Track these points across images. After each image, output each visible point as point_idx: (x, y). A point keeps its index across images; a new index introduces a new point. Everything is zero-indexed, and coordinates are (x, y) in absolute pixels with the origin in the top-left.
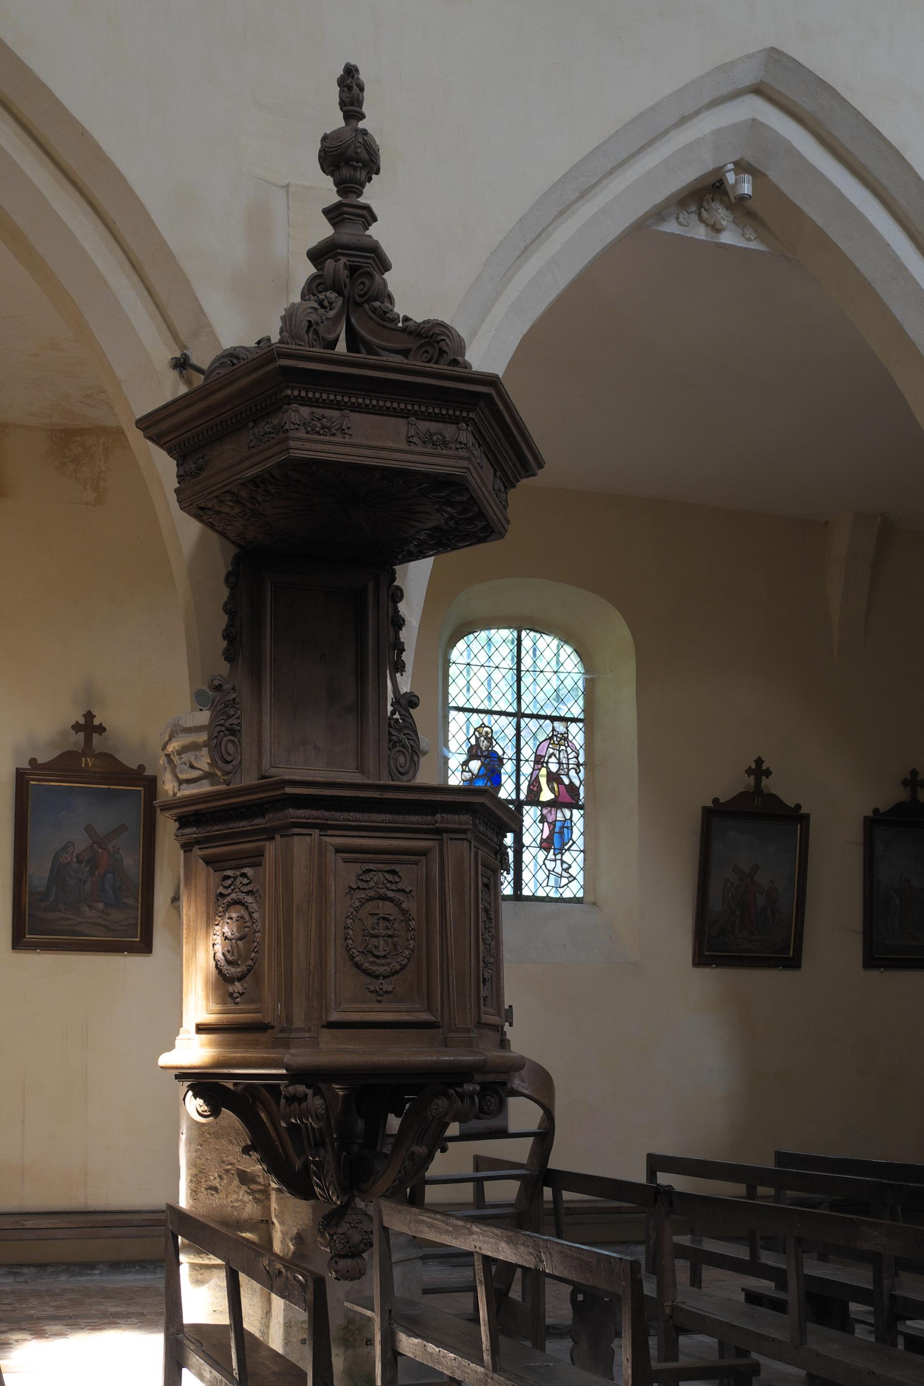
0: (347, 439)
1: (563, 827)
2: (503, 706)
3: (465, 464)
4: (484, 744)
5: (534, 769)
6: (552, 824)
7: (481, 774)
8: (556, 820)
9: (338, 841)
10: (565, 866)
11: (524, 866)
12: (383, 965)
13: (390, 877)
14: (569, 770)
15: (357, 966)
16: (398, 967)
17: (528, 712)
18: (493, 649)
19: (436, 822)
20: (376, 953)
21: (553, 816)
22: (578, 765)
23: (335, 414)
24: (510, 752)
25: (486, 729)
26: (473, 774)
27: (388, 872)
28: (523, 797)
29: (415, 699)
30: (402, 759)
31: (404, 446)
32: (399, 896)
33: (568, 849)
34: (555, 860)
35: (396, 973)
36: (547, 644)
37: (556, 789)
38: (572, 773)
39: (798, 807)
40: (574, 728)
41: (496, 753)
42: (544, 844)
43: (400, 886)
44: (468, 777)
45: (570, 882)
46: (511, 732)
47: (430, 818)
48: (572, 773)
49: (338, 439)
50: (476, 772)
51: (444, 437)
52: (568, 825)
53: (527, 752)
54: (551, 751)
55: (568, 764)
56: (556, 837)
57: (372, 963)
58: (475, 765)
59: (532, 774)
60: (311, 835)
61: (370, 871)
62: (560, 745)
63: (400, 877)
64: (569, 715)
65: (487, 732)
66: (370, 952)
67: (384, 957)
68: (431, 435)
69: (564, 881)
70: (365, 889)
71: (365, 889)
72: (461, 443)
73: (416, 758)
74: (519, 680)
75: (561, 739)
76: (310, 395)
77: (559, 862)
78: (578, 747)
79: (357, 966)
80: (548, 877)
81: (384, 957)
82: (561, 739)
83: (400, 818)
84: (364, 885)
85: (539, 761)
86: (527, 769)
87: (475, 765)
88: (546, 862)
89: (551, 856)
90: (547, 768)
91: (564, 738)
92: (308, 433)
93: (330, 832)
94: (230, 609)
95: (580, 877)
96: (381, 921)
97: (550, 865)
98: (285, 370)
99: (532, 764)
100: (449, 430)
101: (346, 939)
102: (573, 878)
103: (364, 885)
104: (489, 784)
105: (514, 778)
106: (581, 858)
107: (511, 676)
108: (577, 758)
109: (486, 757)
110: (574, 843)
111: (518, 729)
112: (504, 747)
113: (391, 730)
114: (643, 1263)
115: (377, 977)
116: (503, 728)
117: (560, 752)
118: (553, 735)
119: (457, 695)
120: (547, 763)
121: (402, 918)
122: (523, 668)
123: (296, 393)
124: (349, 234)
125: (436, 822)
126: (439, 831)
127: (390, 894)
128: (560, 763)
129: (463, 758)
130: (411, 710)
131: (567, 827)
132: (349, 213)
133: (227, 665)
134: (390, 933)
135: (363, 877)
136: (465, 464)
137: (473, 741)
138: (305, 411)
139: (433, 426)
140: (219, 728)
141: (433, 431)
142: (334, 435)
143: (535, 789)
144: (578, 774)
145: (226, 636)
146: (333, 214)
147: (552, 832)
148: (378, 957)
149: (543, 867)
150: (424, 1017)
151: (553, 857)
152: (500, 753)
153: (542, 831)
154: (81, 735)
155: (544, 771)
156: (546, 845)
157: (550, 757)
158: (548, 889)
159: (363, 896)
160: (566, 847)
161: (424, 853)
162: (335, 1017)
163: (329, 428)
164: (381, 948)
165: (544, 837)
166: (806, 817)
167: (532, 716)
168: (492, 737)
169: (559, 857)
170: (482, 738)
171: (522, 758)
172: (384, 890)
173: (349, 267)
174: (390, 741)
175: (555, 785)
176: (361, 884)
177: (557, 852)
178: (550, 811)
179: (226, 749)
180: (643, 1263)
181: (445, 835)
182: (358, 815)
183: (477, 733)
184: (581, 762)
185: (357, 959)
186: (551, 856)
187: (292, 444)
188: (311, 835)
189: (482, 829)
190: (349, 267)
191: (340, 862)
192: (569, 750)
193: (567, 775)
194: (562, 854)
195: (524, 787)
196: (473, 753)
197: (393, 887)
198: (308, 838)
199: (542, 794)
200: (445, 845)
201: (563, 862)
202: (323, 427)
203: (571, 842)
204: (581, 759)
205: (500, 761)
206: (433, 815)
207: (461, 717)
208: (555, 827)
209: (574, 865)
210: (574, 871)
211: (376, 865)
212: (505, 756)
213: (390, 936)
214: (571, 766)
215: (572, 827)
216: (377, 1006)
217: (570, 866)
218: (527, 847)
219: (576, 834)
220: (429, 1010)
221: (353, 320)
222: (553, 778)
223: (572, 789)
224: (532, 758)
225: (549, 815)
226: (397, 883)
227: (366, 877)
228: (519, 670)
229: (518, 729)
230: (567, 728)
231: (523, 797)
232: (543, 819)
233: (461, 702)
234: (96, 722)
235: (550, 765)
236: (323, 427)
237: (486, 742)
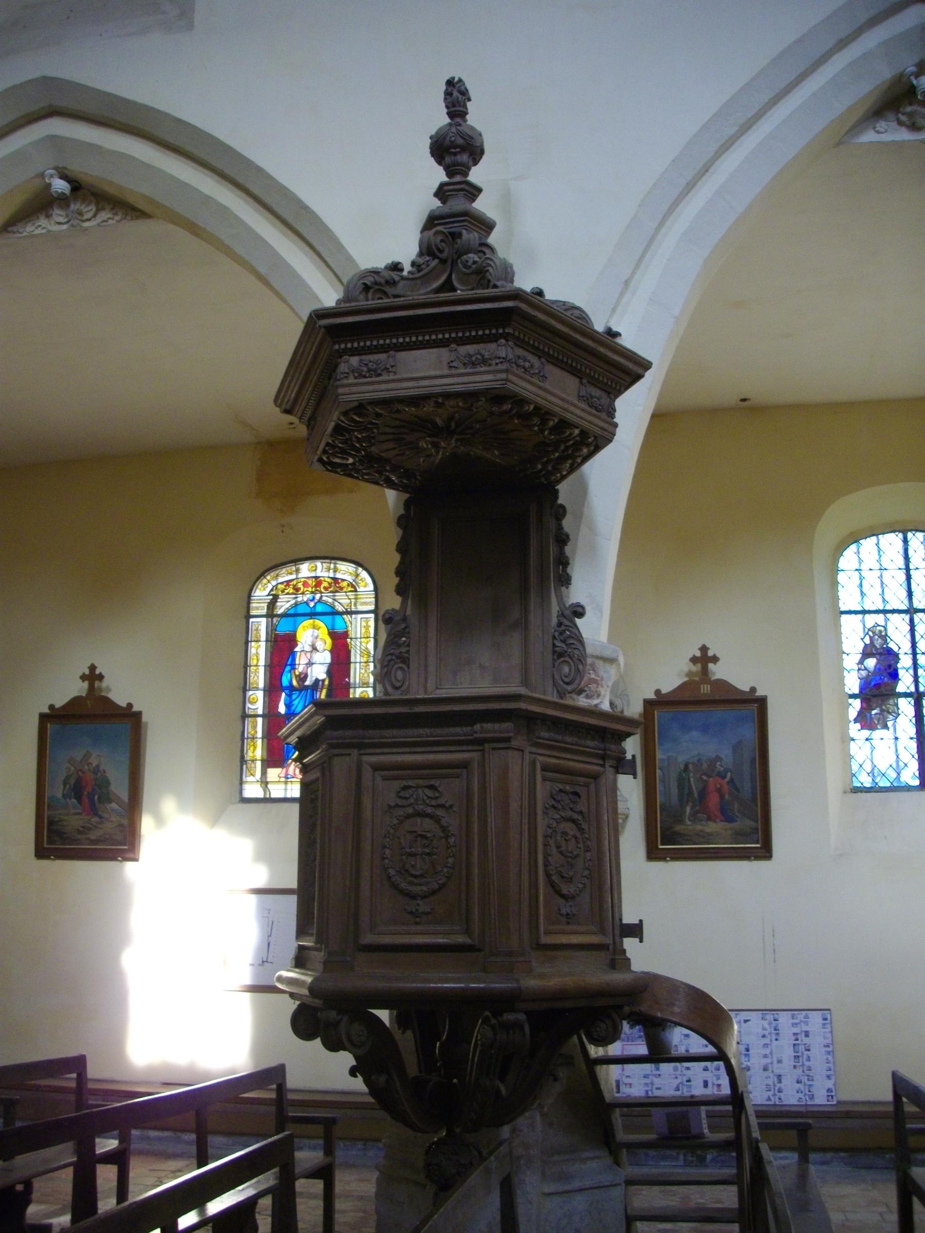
0: (392, 377)
3: (504, 376)
4: (878, 643)
9: (374, 759)
12: (420, 885)
13: (429, 793)
15: (395, 886)
16: (436, 886)
19: (475, 732)
20: (414, 872)
23: (382, 356)
24: (906, 646)
25: (879, 628)
27: (427, 787)
29: (580, 610)
30: (566, 669)
31: (446, 372)
32: (440, 812)
35: (434, 892)
39: (130, 705)
43: (441, 801)
47: (469, 729)
49: (385, 377)
51: (483, 356)
57: (411, 883)
58: (871, 663)
60: (349, 755)
61: (410, 787)
63: (439, 791)
65: (880, 631)
66: (407, 871)
67: (422, 876)
68: (471, 356)
70: (403, 806)
71: (403, 806)
72: (499, 358)
73: (580, 667)
74: (909, 578)
76: (356, 345)
79: (395, 886)
81: (422, 876)
83: (438, 731)
84: (404, 802)
87: (871, 663)
92: (356, 378)
93: (368, 751)
94: (402, 548)
96: (419, 839)
98: (330, 329)
100: (488, 349)
101: (384, 858)
103: (404, 802)
105: (911, 671)
107: (902, 576)
111: (912, 621)
112: (899, 640)
113: (555, 642)
115: (413, 897)
119: (848, 598)
121: (442, 835)
122: (911, 566)
123: (343, 346)
124: (457, 204)
125: (475, 732)
126: (481, 742)
127: (429, 810)
130: (577, 620)
132: (457, 189)
133: (399, 599)
134: (427, 851)
135: (403, 794)
136: (504, 376)
137: (867, 640)
138: (354, 361)
139: (470, 349)
140: (389, 657)
141: (471, 353)
142: (380, 375)
145: (398, 572)
146: (442, 193)
148: (416, 877)
150: (461, 939)
152: (895, 649)
154: (699, 666)
159: (401, 813)
161: (465, 765)
162: (368, 939)
163: (375, 370)
164: (418, 866)
166: (139, 714)
171: (918, 651)
172: (421, 807)
173: (456, 232)
174: (554, 652)
176: (399, 802)
179: (395, 677)
181: (487, 746)
182: (395, 732)
183: (870, 633)
185: (393, 879)
187: (340, 391)
188: (349, 755)
190: (456, 232)
191: (379, 779)
197: (433, 803)
198: (347, 759)
200: (487, 755)
202: (369, 370)
206: (472, 725)
211: (416, 781)
212: (900, 652)
213: (428, 854)
216: (414, 928)
220: (468, 932)
221: (453, 276)
226: (437, 798)
227: (405, 794)
228: (908, 569)
234: (710, 653)
236: (369, 370)
237: (880, 640)
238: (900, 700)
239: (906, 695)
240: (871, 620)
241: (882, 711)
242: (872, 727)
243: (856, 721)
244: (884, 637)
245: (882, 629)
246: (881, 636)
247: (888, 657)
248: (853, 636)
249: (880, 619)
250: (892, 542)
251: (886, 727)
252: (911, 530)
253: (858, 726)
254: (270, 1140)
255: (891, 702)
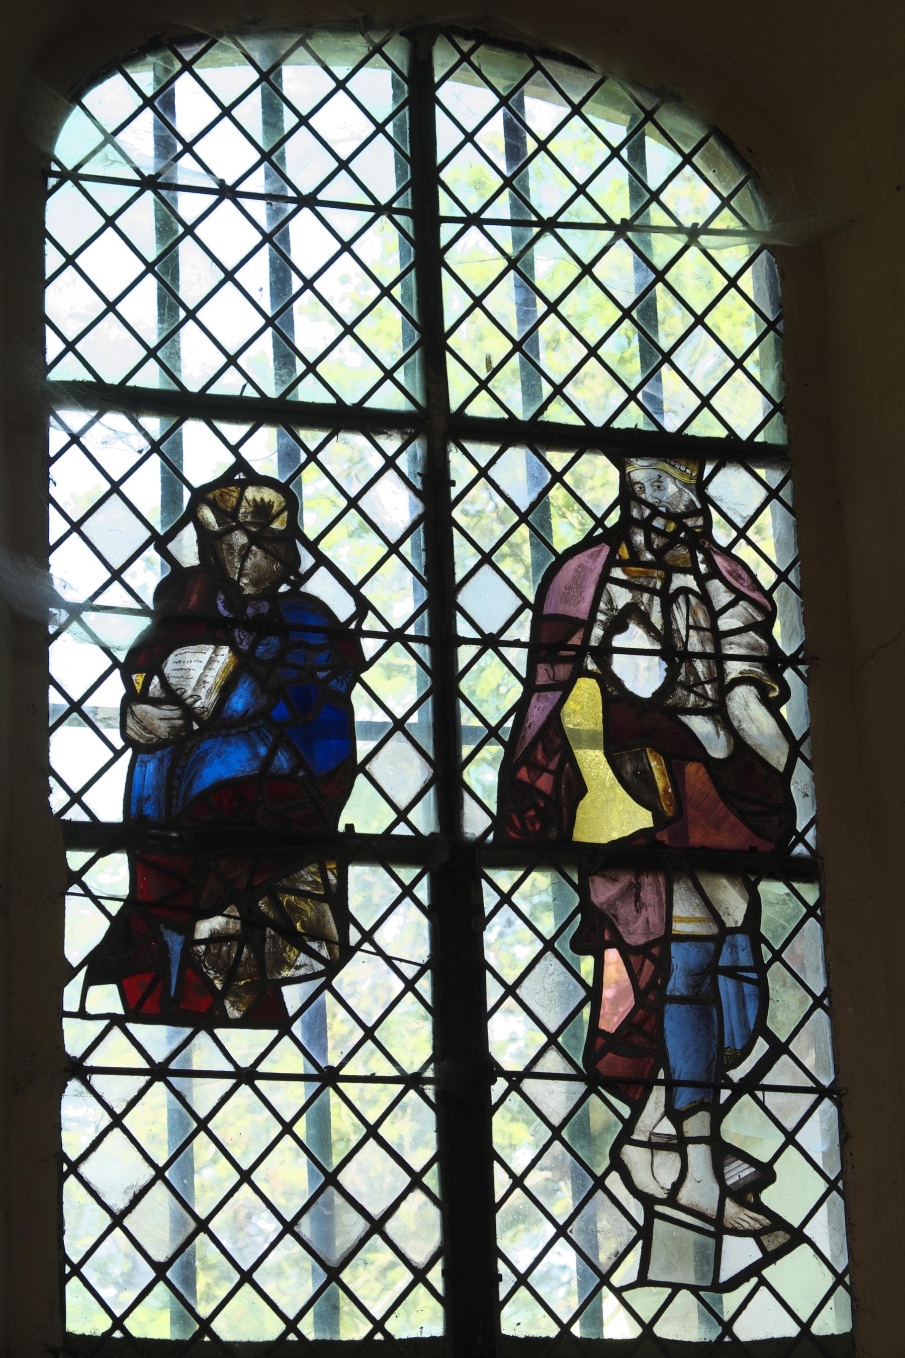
1: (707, 972)
2: (350, 377)
4: (249, 567)
5: (529, 684)
6: (649, 960)
7: (239, 702)
8: (669, 937)
10: (738, 1172)
11: (501, 1181)
14: (725, 688)
17: (483, 408)
18: (352, 1225)
21: (653, 915)
22: (773, 661)
24: (397, 597)
26: (188, 712)
28: (476, 822)
33: (752, 1085)
34: (678, 1145)
36: (579, 141)
37: (661, 783)
38: (745, 705)
40: (736, 489)
41: (318, 606)
42: (611, 1064)
44: (163, 729)
45: (770, 1258)
46: (395, 505)
48: (745, 705)
50: (205, 700)
52: (744, 957)
53: (486, 602)
54: (622, 597)
55: (719, 659)
56: (677, 1029)
58: (200, 669)
59: (520, 709)
62: (669, 571)
64: (706, 427)
65: (262, 510)
69: (739, 1253)
74: (427, 261)
75: (672, 540)
77: (698, 1155)
78: (767, 577)
80: (644, 1234)
82: (672, 540)
85: (559, 646)
86: (492, 688)
88: (633, 1155)
89: (654, 1118)
90: (609, 683)
91: (689, 534)
95: (824, 1230)
97: (655, 1172)
99: (519, 657)
102: (782, 1237)
104: (282, 761)
106: (819, 1135)
108: (764, 628)
109: (260, 627)
110: (778, 1049)
114: (694, 499)
116: (355, 526)
117: (668, 600)
118: (626, 519)
120: (605, 652)
128: (670, 650)
129: (127, 632)
131: (732, 972)
137: (187, 548)
143: (545, 783)
144: (773, 706)
147: (649, 997)
149: (614, 1182)
151: (667, 1128)
152: (342, 607)
153: (594, 994)
155: (584, 707)
156: (614, 1063)
157: (617, 624)
158: (646, 1301)
160: (737, 1074)
165: (610, 1022)
167: (504, 432)
168: (294, 530)
169: (697, 1125)
170: (240, 539)
175: (656, 765)
177: (684, 1098)
178: (634, 892)
180: (694, 499)
183: (207, 514)
184: (788, 650)
186: (654, 1118)
189: (238, 639)
192: (720, 595)
193: (719, 714)
194: (719, 1113)
195: (483, 775)
196: (181, 613)
199: (586, 810)
201: (723, 1153)
203: (761, 1047)
204: (786, 635)
205: (339, 650)
207: (117, 438)
208: (664, 967)
209: (790, 1166)
210: (794, 1192)
212: (370, 623)
214: (734, 669)
215: (762, 968)
217: (765, 1174)
218: (515, 1080)
219: (786, 1007)
222: (632, 728)
223: (748, 778)
224: (522, 630)
225: (625, 910)
229: (430, 339)
230: (701, 486)
231: (476, 822)
232: (591, 931)
233: (112, 356)
235: (620, 665)
237: (257, 557)
238: (355, 872)
239: (383, 850)
240: (204, 454)
241: (252, 924)
242: (200, 1014)
243: (99, 967)
244: (283, 541)
245: (268, 495)
246: (261, 536)
247: (300, 660)
248: (106, 517)
249: (264, 449)
250: (344, 101)
251: (269, 1014)
252: (451, 33)
253: (106, 998)
254: (174, 971)
255: (308, 876)
